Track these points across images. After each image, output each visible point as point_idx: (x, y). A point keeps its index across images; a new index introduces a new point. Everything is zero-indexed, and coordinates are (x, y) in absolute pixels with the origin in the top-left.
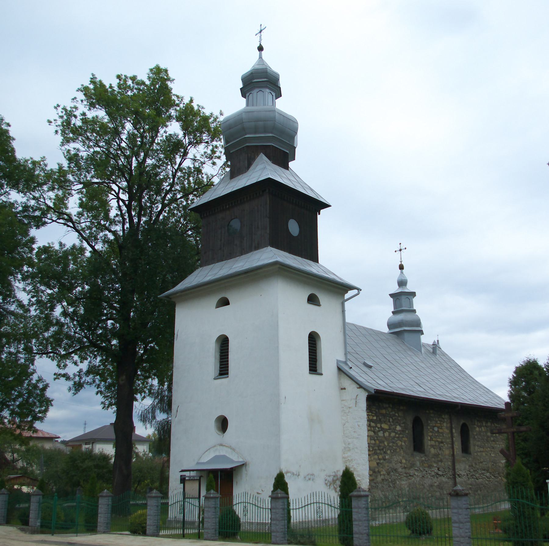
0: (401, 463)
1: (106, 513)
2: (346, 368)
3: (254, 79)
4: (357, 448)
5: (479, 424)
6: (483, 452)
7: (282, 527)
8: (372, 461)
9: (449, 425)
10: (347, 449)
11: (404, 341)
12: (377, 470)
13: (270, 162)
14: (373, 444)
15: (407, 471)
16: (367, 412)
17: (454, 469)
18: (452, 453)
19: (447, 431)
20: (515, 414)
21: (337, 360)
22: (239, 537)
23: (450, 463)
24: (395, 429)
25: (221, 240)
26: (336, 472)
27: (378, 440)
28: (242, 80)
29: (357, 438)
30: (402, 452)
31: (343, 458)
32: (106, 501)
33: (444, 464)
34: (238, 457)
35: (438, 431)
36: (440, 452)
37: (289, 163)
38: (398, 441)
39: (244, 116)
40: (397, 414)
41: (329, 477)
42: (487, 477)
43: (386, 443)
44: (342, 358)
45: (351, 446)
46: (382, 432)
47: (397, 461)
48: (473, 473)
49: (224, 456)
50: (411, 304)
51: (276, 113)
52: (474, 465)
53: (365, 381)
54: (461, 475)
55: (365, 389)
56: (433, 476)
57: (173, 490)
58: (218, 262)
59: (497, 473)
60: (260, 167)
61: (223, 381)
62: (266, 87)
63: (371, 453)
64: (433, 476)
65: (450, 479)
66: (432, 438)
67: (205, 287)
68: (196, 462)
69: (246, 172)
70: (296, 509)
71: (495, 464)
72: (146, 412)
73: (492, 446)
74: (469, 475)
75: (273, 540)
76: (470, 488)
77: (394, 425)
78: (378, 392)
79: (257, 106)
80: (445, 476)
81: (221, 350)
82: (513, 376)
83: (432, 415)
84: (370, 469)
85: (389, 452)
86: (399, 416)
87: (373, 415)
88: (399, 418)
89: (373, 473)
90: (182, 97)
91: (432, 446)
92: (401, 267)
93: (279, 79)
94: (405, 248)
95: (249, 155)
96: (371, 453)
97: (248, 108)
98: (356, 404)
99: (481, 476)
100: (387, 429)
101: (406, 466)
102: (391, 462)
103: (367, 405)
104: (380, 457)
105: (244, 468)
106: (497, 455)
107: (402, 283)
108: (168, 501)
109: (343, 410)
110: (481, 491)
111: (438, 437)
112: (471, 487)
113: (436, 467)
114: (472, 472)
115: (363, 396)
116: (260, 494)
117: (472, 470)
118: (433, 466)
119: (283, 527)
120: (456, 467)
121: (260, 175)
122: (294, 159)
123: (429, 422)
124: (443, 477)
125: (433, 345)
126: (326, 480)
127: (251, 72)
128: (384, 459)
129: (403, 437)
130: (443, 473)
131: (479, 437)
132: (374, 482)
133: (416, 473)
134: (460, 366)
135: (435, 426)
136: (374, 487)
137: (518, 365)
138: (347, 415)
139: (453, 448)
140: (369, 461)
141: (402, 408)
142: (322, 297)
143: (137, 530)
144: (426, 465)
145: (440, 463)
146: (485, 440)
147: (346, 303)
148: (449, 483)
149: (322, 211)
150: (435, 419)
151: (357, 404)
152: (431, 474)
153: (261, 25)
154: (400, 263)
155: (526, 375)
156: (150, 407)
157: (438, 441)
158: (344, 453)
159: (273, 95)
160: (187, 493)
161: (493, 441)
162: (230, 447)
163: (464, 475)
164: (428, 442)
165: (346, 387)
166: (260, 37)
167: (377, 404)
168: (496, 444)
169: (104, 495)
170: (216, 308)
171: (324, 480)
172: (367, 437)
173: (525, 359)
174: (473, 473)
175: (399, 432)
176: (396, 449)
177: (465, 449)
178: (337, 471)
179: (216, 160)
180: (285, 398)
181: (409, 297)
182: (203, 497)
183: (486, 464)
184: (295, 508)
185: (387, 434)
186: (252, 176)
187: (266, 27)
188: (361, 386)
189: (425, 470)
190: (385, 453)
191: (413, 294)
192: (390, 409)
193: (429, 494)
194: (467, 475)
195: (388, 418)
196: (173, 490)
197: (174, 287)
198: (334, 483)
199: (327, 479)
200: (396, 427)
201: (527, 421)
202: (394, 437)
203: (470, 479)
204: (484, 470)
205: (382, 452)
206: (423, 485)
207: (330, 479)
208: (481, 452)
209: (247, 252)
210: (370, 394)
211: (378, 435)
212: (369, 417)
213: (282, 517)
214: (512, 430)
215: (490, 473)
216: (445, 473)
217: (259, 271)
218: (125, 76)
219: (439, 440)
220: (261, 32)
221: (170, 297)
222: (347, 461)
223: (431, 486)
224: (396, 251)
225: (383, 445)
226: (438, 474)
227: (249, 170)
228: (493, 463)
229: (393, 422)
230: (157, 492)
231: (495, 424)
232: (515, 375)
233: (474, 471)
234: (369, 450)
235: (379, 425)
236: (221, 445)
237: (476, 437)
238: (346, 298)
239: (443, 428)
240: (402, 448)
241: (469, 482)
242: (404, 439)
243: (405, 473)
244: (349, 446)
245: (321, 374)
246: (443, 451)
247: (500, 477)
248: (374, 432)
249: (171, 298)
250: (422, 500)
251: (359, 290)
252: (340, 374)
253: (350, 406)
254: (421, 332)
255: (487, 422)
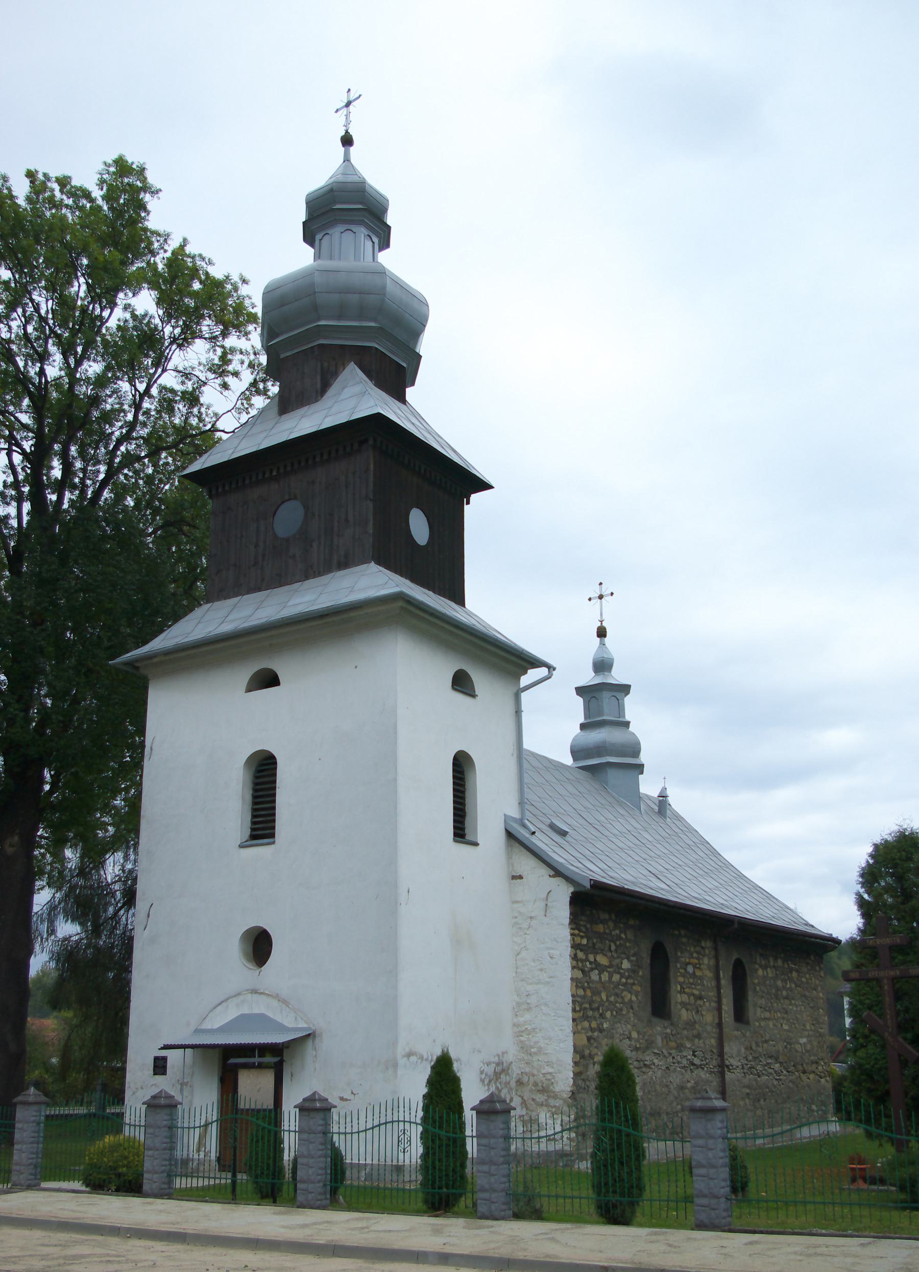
0: (630, 1038)
1: (32, 1143)
2: (523, 833)
3: (335, 203)
4: (546, 1004)
5: (763, 962)
6: (769, 1019)
7: (320, 1172)
8: (579, 1033)
9: (712, 962)
10: (523, 1006)
11: (607, 785)
12: (587, 1052)
13: (370, 384)
14: (580, 996)
15: (640, 1056)
16: (572, 929)
17: (721, 1054)
18: (717, 1021)
19: (709, 974)
20: (898, 941)
21: (505, 815)
22: (341, 1198)
23: (713, 1041)
24: (619, 967)
25: (256, 546)
26: (500, 1054)
27: (590, 988)
28: (307, 203)
29: (548, 983)
30: (632, 1015)
31: (515, 1025)
32: (35, 1114)
33: (704, 1043)
34: (296, 1018)
35: (694, 973)
36: (697, 1018)
37: (407, 389)
38: (625, 993)
39: (318, 279)
40: (623, 936)
41: (488, 1065)
42: (776, 1072)
43: (604, 997)
44: (514, 813)
45: (533, 1000)
46: (597, 972)
47: (624, 1034)
48: (752, 1063)
49: (262, 1017)
50: (621, 709)
51: (388, 281)
52: (754, 1048)
53: (566, 862)
54: (732, 1066)
55: (568, 879)
56: (684, 1067)
57: (134, 1090)
58: (248, 593)
59: (792, 1064)
60: (347, 392)
61: (261, 852)
62: (361, 223)
63: (577, 1015)
64: (684, 1067)
65: (714, 1075)
66: (684, 988)
67: (219, 646)
68: (193, 1027)
69: (317, 401)
70: (352, 1133)
71: (788, 1046)
72: (37, 920)
73: (784, 1008)
74: (746, 1067)
75: (300, 1198)
76: (748, 1094)
77: (618, 957)
78: (597, 885)
79: (340, 259)
80: (706, 1069)
81: (255, 784)
82: (868, 862)
83: (684, 940)
84: (576, 1050)
85: (608, 1014)
86: (627, 940)
87: (582, 934)
88: (628, 944)
89: (580, 1059)
90: (168, 235)
91: (684, 1005)
92: (602, 633)
93: (387, 210)
94: (612, 594)
95: (326, 364)
96: (577, 1015)
97: (319, 262)
98: (546, 911)
99: (765, 1070)
100: (605, 966)
101: (638, 1046)
102: (612, 1037)
103: (571, 914)
104: (594, 1025)
105: (310, 1043)
106: (793, 1026)
107: (602, 665)
108: (122, 1111)
109: (516, 923)
110: (765, 1100)
111: (693, 986)
112: (748, 1091)
113: (689, 1048)
114: (750, 1061)
115: (563, 893)
116: (346, 1100)
117: (750, 1058)
118: (686, 1047)
119: (323, 1172)
120: (726, 1049)
121: (355, 408)
122: (413, 384)
123: (679, 954)
124: (700, 1070)
125: (659, 797)
126: (482, 1072)
127: (329, 187)
128: (601, 1030)
129: (634, 984)
130: (702, 1063)
131: (762, 988)
132: (582, 1077)
133: (655, 1061)
134: (708, 843)
135: (689, 963)
136: (581, 1088)
137: (878, 840)
138: (526, 934)
139: (719, 1009)
140: (574, 1034)
141: (632, 922)
142: (480, 679)
143: (104, 1181)
144: (673, 1044)
145: (696, 1041)
146: (773, 996)
147: (524, 696)
148: (712, 1082)
149: (474, 497)
150: (688, 949)
151: (548, 911)
152: (681, 1063)
153: (349, 90)
154: (599, 624)
155: (898, 861)
156: (45, 908)
157: (693, 995)
158: (516, 1015)
159: (373, 243)
160: (243, 1098)
161: (786, 998)
162: (277, 997)
163: (738, 1067)
164: (677, 997)
165: (524, 875)
166: (346, 115)
167: (588, 913)
168: (791, 1004)
169: (31, 1099)
170: (246, 692)
171: (479, 1072)
172: (570, 981)
173: (896, 828)
174: (752, 1063)
175: (627, 974)
176: (621, 1010)
177: (740, 1015)
178: (503, 1053)
179: (230, 380)
180: (409, 892)
181: (619, 695)
182: (472, 1109)
183: (774, 1046)
184: (186, 1125)
185: (605, 977)
186: (333, 410)
187: (360, 96)
188: (557, 872)
189: (670, 1054)
190: (602, 1016)
191: (625, 689)
192: (611, 924)
193: (678, 1104)
194: (743, 1068)
195: (607, 942)
196: (134, 1090)
197: (145, 642)
198: (497, 1080)
199: (483, 1070)
200: (622, 963)
201: (900, 957)
202: (619, 983)
203: (747, 1076)
204: (771, 1057)
205: (597, 1014)
206: (667, 1086)
207: (490, 1070)
208: (765, 1019)
209: (319, 574)
210: (578, 889)
211: (590, 978)
212: (576, 939)
213: (504, 1156)
214: (892, 973)
215: (781, 1063)
216: (705, 1062)
217: (352, 614)
218: (45, 175)
219: (696, 992)
220: (348, 104)
221: (137, 664)
222: (523, 1032)
223: (682, 1088)
224: (590, 599)
225: (599, 1000)
226: (693, 1064)
227: (325, 397)
228: (785, 1044)
229: (616, 951)
230: (37, 1092)
231: (789, 962)
232: (871, 861)
233: (755, 1058)
234: (574, 1010)
235: (591, 957)
236: (254, 991)
237: (758, 988)
238: (522, 686)
239: (702, 966)
240: (632, 1008)
241: (746, 1081)
242: (635, 988)
243: (638, 1061)
244: (529, 1001)
245: (476, 844)
246: (702, 1015)
247: (797, 1072)
248: (583, 971)
249: (137, 668)
250: (664, 1117)
251: (551, 668)
252: (511, 846)
253: (533, 915)
254: (640, 768)
255: (776, 959)
